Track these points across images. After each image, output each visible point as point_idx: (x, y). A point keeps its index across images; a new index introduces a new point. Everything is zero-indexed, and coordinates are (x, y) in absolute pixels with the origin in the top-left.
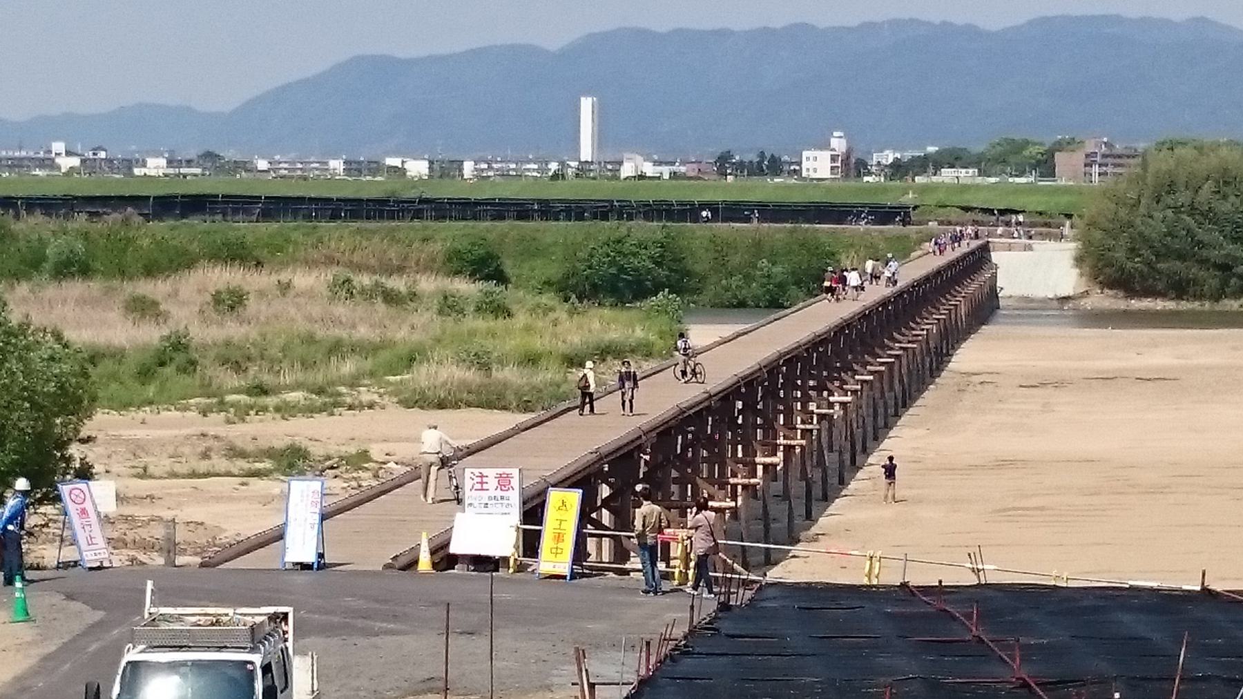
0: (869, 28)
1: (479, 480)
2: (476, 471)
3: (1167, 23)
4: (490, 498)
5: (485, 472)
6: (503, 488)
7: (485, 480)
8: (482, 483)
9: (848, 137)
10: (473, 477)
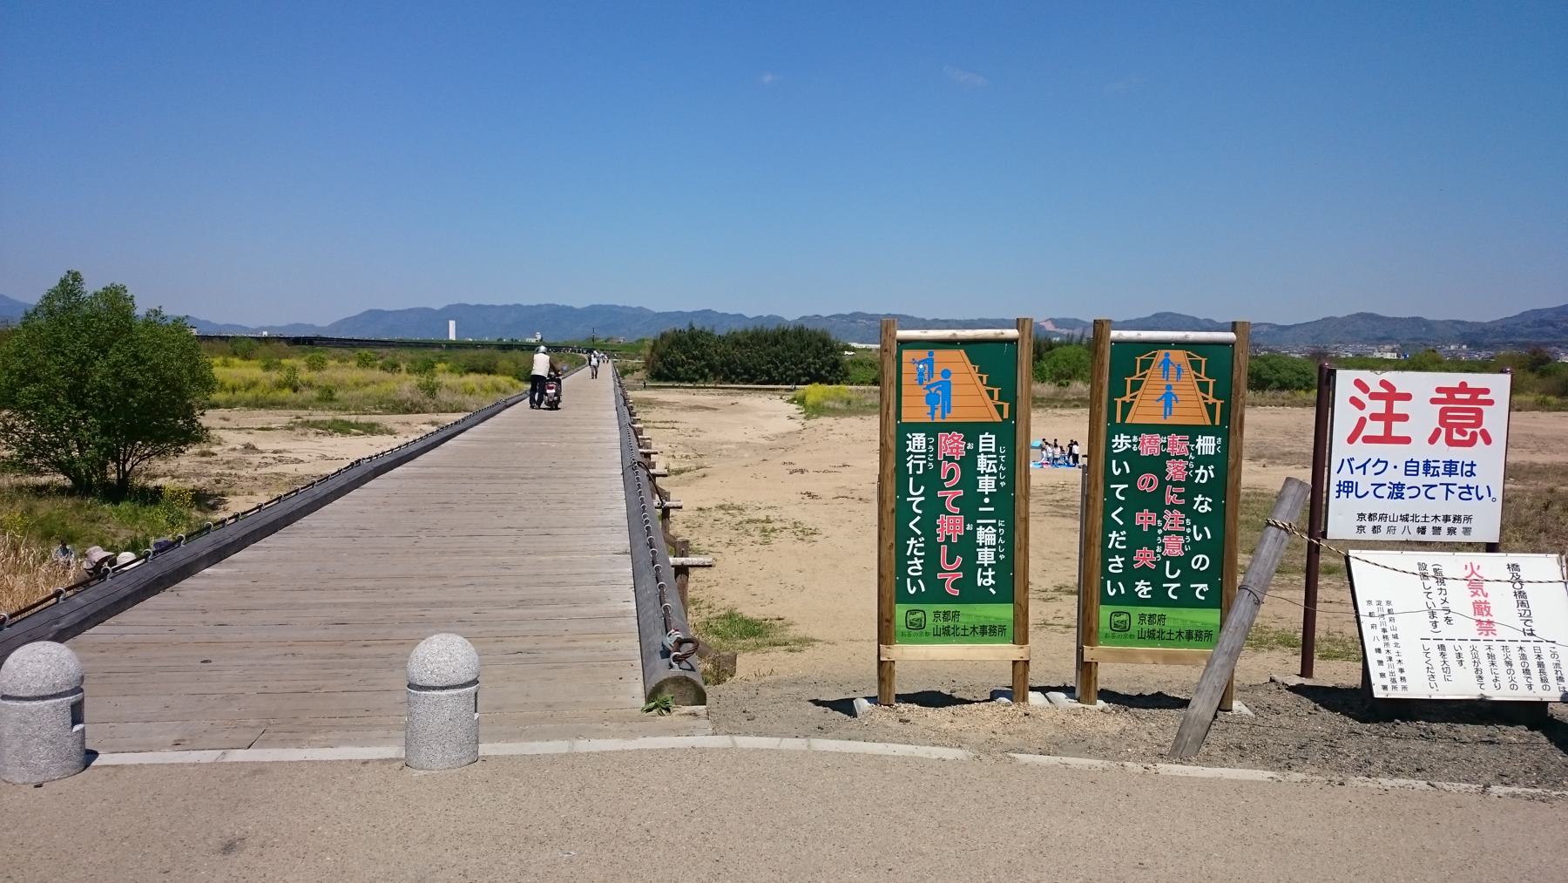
0: (539, 306)
1: (1380, 407)
2: (1372, 379)
3: (630, 308)
4: (1411, 467)
5: (1402, 380)
6: (1456, 436)
7: (1399, 407)
8: (1389, 417)
9: (541, 334)
10: (1364, 397)
